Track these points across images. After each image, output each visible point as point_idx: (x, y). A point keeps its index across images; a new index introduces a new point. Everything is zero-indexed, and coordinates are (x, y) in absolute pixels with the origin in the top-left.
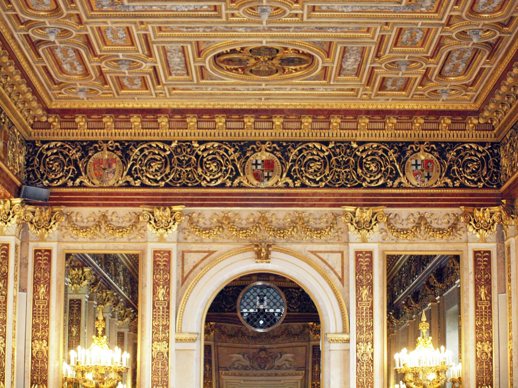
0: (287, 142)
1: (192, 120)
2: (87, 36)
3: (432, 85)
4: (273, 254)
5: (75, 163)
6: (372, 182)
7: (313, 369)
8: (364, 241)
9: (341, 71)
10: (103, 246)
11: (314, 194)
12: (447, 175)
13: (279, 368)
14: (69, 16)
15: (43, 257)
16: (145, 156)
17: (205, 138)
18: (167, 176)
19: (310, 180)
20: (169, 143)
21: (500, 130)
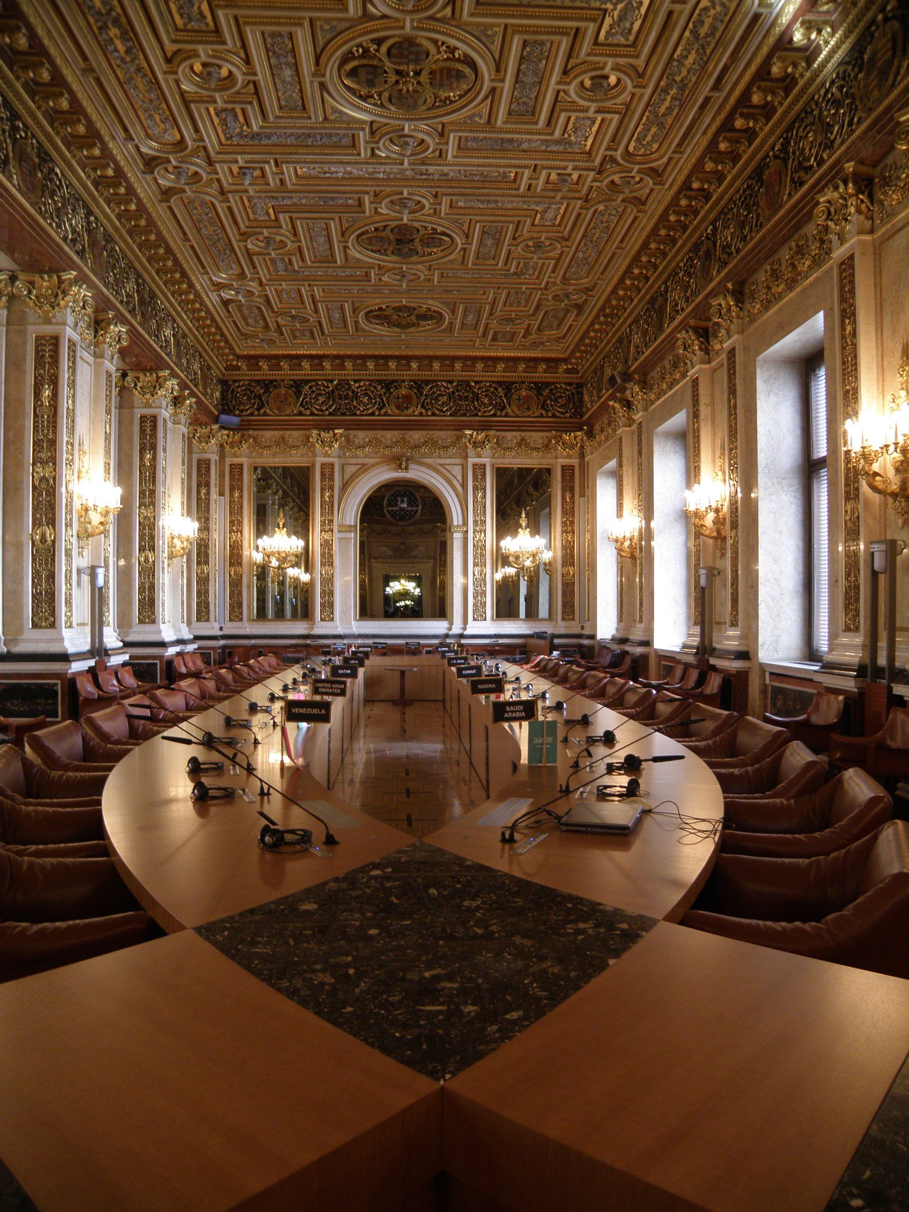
0: (421, 381)
1: (349, 364)
2: (266, 296)
4: (411, 466)
5: (260, 397)
6: (485, 412)
7: (441, 558)
8: (479, 456)
9: (463, 325)
10: (282, 460)
11: (442, 421)
12: (543, 407)
13: (415, 557)
14: (252, 280)
15: (237, 470)
16: (313, 392)
17: (358, 378)
18: (330, 407)
19: (438, 410)
20: (332, 381)
21: (584, 373)
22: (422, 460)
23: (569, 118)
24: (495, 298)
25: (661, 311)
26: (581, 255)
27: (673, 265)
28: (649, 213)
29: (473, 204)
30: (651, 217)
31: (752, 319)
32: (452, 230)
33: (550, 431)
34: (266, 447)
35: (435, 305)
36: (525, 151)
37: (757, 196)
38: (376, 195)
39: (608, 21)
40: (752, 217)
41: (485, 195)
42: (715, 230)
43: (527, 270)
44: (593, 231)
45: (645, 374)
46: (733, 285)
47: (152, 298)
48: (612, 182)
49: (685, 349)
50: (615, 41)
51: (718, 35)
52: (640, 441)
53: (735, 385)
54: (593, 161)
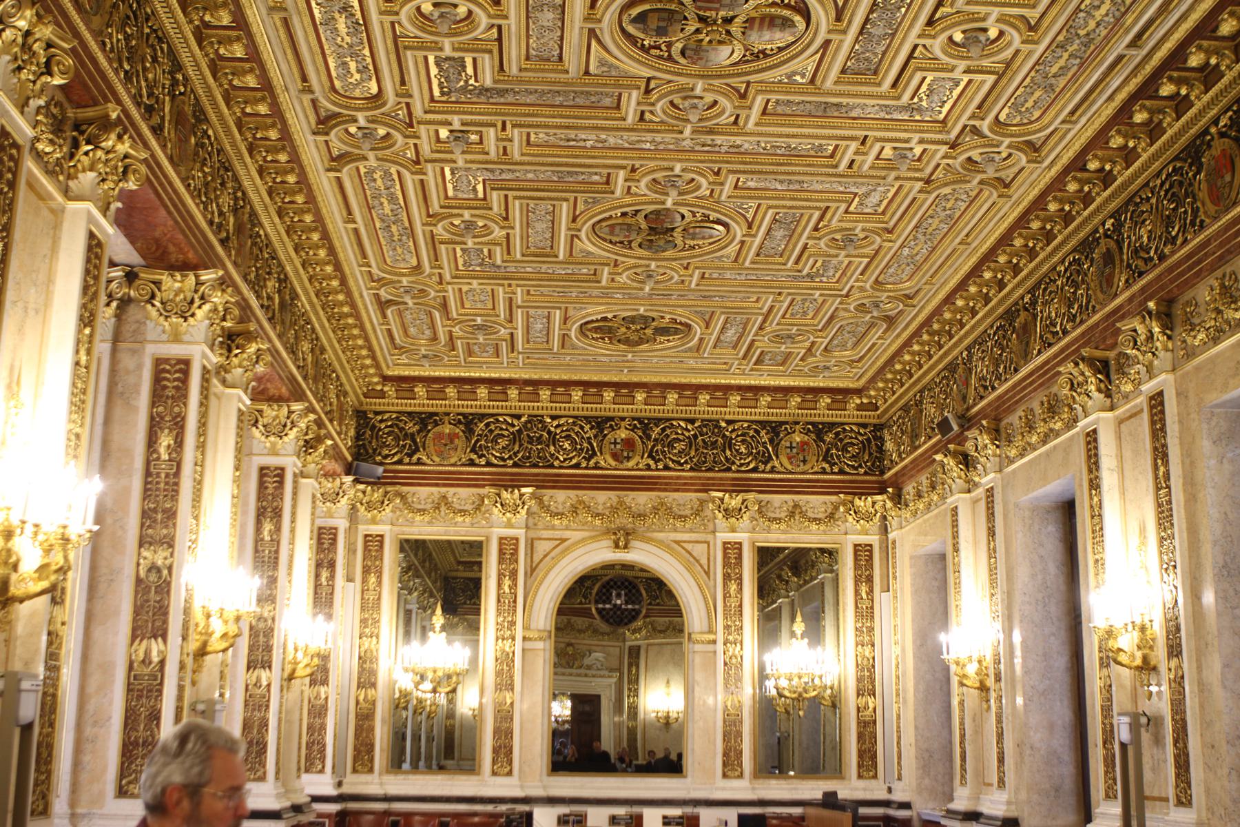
0: (649, 419)
1: (545, 394)
3: (817, 359)
6: (742, 465)
11: (678, 478)
13: (589, 667)
15: (374, 544)
17: (558, 413)
18: (515, 454)
19: (673, 461)
22: (649, 535)
23: (924, 78)
24: (772, 307)
25: (1026, 331)
26: (906, 251)
27: (1045, 268)
28: (1014, 199)
29: (768, 185)
31: (1190, 354)
32: (731, 218)
33: (837, 494)
34: (419, 510)
35: (682, 315)
36: (854, 119)
37: (1191, 185)
40: (1186, 212)
41: (789, 173)
42: (1118, 226)
43: (825, 270)
44: (930, 221)
45: (998, 420)
46: (1157, 304)
47: (292, 299)
48: (969, 159)
49: (1072, 388)
52: (991, 515)
53: (1164, 446)
54: (948, 132)
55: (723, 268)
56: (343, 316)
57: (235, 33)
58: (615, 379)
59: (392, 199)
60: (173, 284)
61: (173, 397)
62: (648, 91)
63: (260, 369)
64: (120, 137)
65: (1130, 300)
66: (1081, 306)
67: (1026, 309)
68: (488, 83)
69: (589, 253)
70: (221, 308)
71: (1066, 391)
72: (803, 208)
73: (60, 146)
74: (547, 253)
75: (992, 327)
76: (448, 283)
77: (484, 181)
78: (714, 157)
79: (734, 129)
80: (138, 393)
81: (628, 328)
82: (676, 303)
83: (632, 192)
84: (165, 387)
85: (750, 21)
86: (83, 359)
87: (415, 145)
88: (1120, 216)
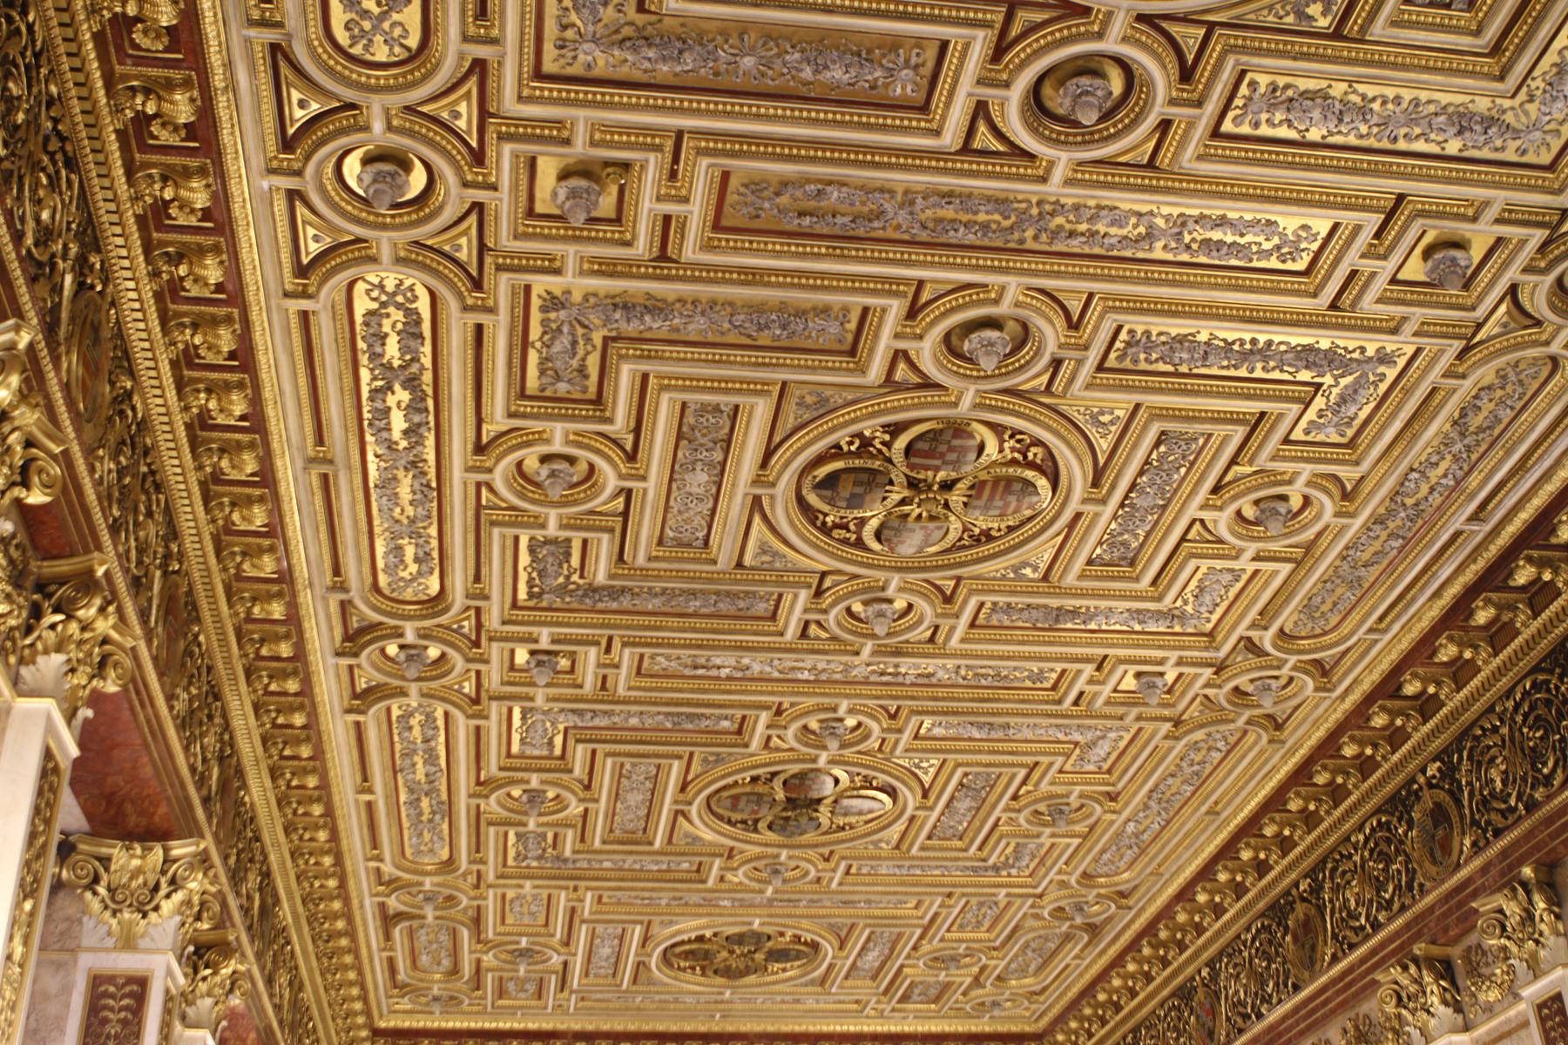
3: (987, 991)
25: (1308, 933)
28: (1288, 745)
30: (1292, 751)
38: (779, 713)
39: (1319, 403)
42: (1449, 771)
43: (1017, 859)
46: (1535, 871)
50: (1321, 438)
51: (1497, 432)
54: (1217, 649)
55: (880, 858)
56: (334, 935)
57: (257, 492)
58: (703, 1029)
59: (431, 758)
60: (127, 860)
61: (116, 1036)
62: (819, 593)
63: (236, 1001)
64: (102, 610)
65: (1484, 870)
66: (1398, 887)
67: (1304, 900)
68: (601, 578)
69: (696, 839)
70: (196, 899)
71: (1390, 1009)
72: (1003, 765)
73: (20, 607)
74: (638, 839)
75: (1248, 929)
76: (490, 886)
77: (566, 729)
78: (894, 691)
79: (929, 648)
80: (62, 1032)
81: (732, 952)
82: (805, 911)
83: (769, 744)
84: (105, 1021)
85: (977, 487)
86: (17, 956)
87: (478, 673)
88: (1450, 757)
